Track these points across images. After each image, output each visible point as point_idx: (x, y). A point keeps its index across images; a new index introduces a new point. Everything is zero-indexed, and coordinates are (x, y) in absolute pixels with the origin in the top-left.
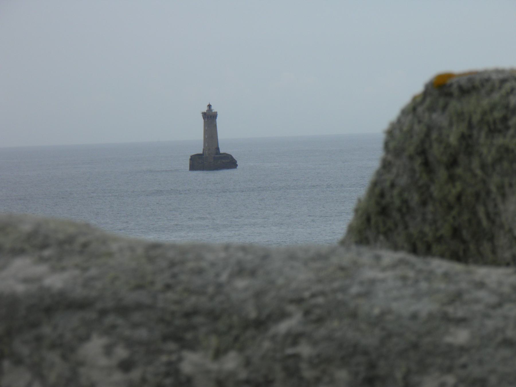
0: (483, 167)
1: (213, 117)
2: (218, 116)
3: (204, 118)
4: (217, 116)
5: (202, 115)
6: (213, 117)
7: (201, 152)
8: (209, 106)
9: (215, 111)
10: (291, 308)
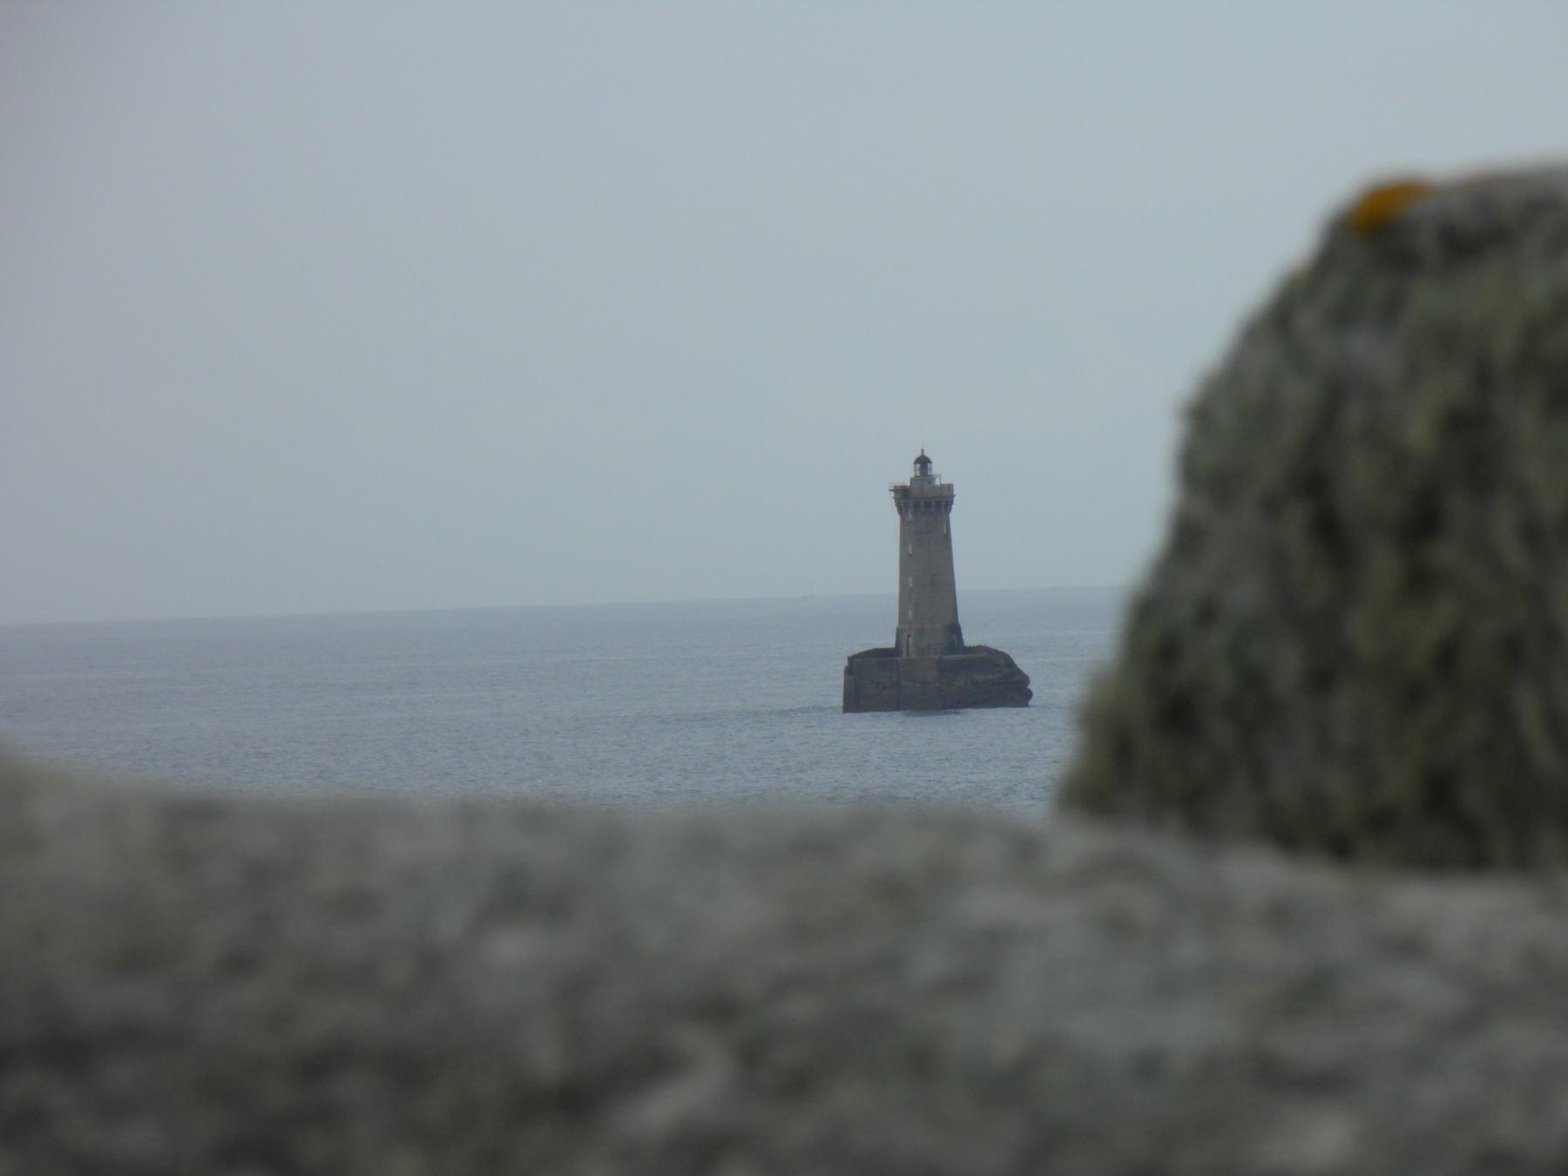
0: (1532, 534)
1: (938, 504)
2: (956, 500)
3: (902, 509)
4: (952, 502)
5: (896, 499)
6: (938, 504)
7: (890, 643)
8: (923, 462)
9: (943, 482)
10: (692, 1039)
